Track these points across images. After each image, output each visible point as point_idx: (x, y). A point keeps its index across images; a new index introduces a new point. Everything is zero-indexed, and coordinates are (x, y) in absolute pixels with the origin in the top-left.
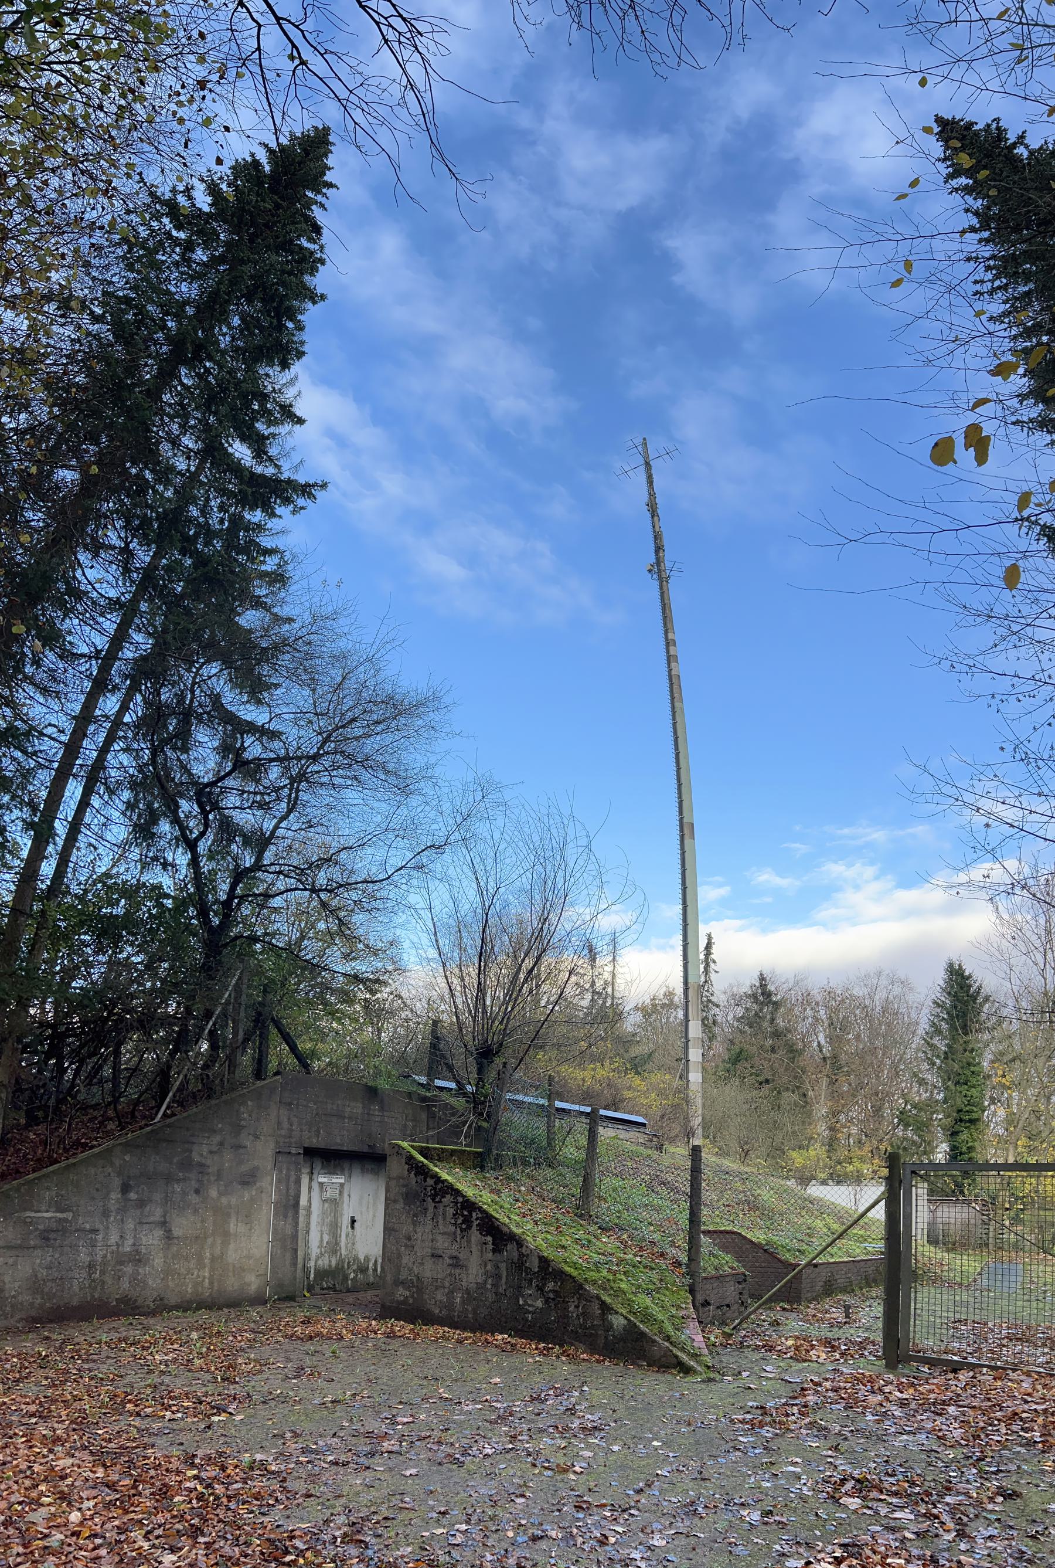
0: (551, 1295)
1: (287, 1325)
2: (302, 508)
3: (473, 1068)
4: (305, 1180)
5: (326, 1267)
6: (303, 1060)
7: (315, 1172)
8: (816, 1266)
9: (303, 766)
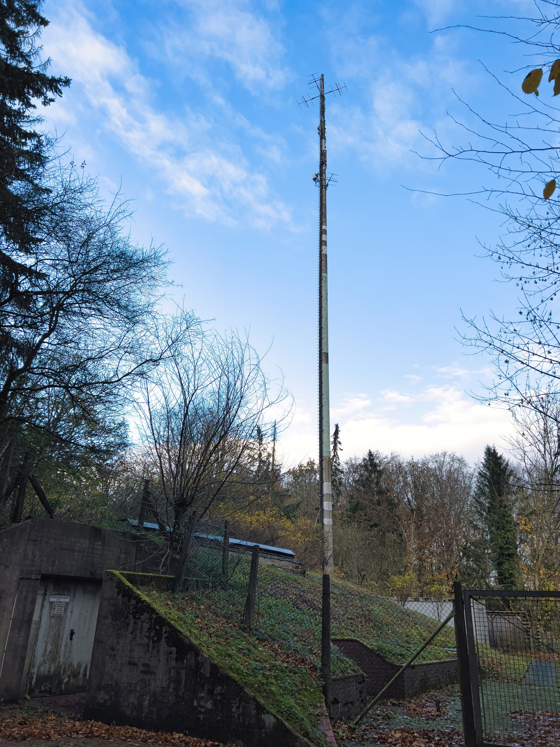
0: (219, 698)
1: (7, 726)
2: (52, 100)
3: (173, 514)
4: (39, 599)
5: (46, 673)
6: (49, 508)
7: (48, 593)
8: (413, 667)
9: (61, 299)
